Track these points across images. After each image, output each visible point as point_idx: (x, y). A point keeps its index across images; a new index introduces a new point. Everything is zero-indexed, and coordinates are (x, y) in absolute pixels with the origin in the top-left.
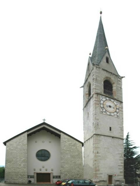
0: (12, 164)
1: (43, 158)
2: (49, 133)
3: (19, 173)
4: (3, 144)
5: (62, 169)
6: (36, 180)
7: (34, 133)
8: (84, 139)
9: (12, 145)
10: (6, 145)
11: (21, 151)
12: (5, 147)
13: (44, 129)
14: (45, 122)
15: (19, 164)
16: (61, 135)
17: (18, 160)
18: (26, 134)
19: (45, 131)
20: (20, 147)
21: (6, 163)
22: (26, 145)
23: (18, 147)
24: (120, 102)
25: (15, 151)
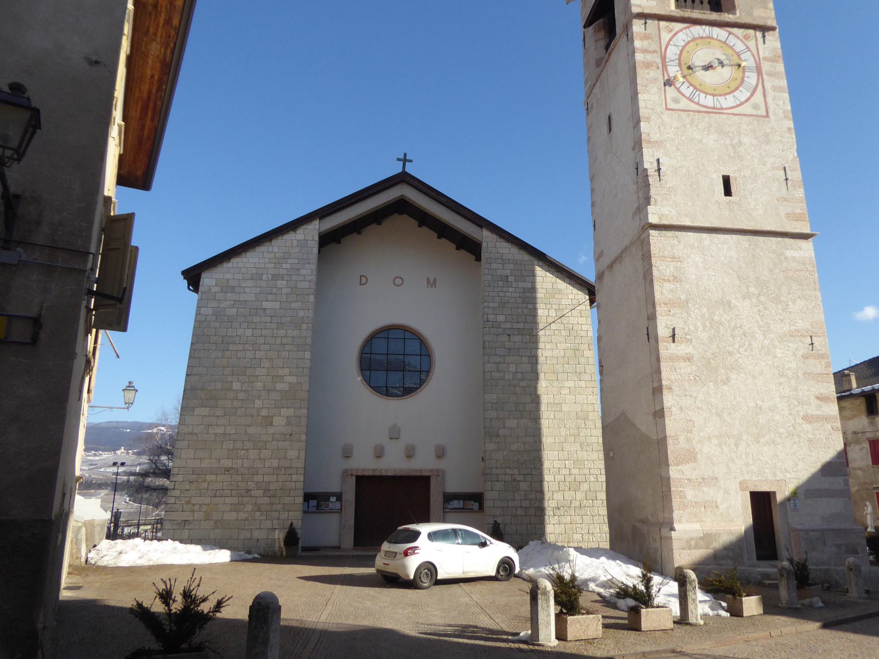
0: (219, 413)
1: (395, 378)
2: (425, 230)
3: (259, 478)
4: (182, 277)
5: (490, 446)
6: (352, 522)
7: (356, 227)
8: (599, 256)
9: (233, 289)
10: (196, 290)
11: (282, 332)
12: (194, 296)
13: (401, 206)
14: (410, 169)
15: (264, 413)
16: (484, 245)
17: (259, 385)
18: (313, 230)
19: (406, 222)
20: (277, 305)
21: (186, 408)
22: (312, 298)
23: (266, 305)
24: (759, 34)
25: (249, 332)
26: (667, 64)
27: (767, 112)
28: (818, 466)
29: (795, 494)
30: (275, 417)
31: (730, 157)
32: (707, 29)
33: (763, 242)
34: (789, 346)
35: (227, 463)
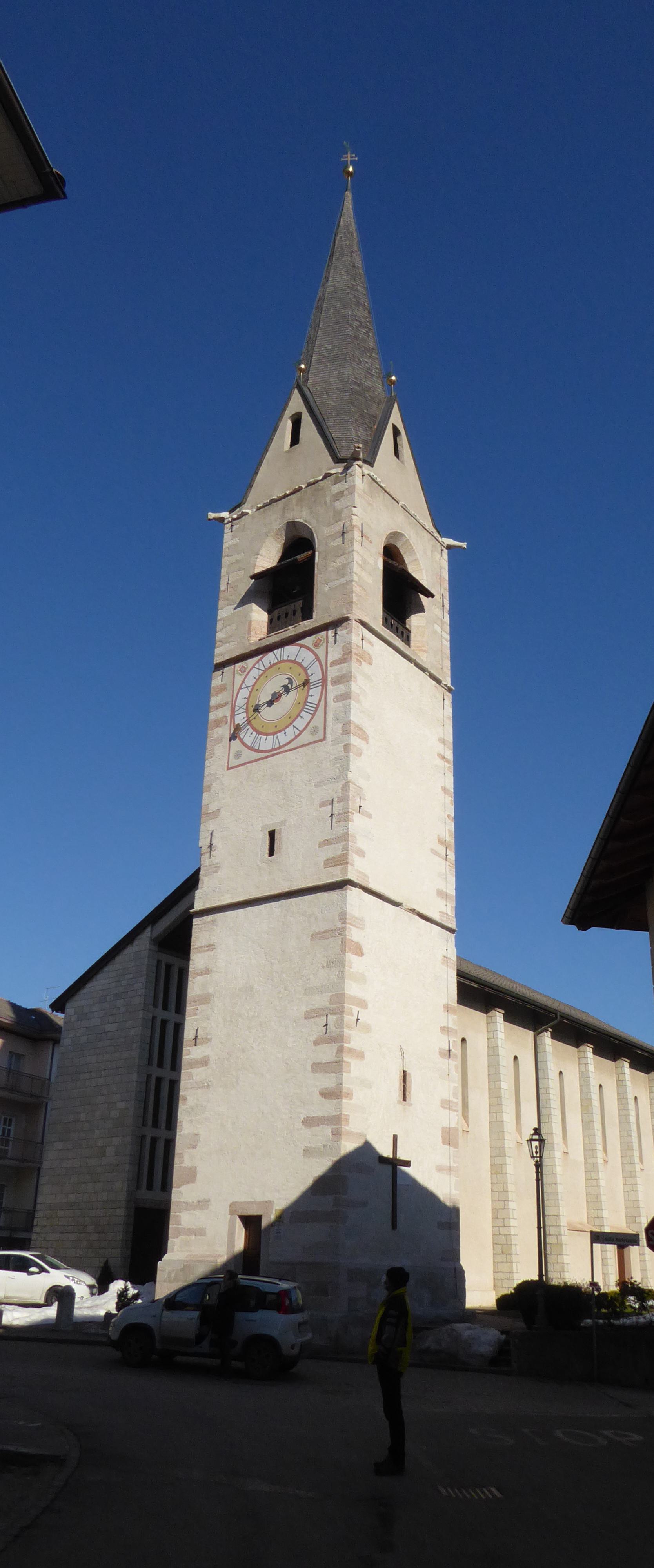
18: (144, 941)
26: (245, 711)
27: (232, 768)
28: (309, 1182)
29: (280, 1218)
30: (108, 1147)
31: (279, 806)
32: (277, 652)
33: (296, 904)
34: (302, 1032)
35: (72, 1198)
